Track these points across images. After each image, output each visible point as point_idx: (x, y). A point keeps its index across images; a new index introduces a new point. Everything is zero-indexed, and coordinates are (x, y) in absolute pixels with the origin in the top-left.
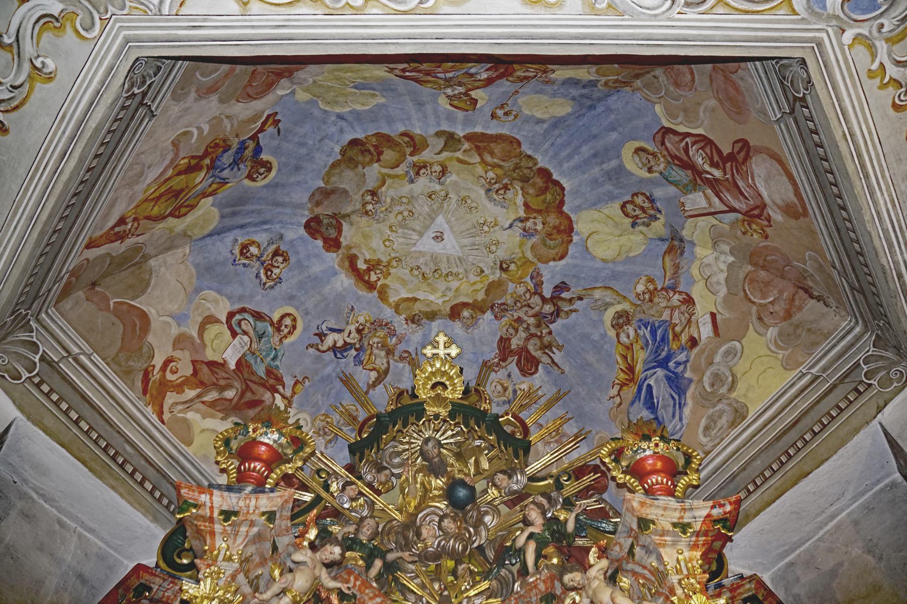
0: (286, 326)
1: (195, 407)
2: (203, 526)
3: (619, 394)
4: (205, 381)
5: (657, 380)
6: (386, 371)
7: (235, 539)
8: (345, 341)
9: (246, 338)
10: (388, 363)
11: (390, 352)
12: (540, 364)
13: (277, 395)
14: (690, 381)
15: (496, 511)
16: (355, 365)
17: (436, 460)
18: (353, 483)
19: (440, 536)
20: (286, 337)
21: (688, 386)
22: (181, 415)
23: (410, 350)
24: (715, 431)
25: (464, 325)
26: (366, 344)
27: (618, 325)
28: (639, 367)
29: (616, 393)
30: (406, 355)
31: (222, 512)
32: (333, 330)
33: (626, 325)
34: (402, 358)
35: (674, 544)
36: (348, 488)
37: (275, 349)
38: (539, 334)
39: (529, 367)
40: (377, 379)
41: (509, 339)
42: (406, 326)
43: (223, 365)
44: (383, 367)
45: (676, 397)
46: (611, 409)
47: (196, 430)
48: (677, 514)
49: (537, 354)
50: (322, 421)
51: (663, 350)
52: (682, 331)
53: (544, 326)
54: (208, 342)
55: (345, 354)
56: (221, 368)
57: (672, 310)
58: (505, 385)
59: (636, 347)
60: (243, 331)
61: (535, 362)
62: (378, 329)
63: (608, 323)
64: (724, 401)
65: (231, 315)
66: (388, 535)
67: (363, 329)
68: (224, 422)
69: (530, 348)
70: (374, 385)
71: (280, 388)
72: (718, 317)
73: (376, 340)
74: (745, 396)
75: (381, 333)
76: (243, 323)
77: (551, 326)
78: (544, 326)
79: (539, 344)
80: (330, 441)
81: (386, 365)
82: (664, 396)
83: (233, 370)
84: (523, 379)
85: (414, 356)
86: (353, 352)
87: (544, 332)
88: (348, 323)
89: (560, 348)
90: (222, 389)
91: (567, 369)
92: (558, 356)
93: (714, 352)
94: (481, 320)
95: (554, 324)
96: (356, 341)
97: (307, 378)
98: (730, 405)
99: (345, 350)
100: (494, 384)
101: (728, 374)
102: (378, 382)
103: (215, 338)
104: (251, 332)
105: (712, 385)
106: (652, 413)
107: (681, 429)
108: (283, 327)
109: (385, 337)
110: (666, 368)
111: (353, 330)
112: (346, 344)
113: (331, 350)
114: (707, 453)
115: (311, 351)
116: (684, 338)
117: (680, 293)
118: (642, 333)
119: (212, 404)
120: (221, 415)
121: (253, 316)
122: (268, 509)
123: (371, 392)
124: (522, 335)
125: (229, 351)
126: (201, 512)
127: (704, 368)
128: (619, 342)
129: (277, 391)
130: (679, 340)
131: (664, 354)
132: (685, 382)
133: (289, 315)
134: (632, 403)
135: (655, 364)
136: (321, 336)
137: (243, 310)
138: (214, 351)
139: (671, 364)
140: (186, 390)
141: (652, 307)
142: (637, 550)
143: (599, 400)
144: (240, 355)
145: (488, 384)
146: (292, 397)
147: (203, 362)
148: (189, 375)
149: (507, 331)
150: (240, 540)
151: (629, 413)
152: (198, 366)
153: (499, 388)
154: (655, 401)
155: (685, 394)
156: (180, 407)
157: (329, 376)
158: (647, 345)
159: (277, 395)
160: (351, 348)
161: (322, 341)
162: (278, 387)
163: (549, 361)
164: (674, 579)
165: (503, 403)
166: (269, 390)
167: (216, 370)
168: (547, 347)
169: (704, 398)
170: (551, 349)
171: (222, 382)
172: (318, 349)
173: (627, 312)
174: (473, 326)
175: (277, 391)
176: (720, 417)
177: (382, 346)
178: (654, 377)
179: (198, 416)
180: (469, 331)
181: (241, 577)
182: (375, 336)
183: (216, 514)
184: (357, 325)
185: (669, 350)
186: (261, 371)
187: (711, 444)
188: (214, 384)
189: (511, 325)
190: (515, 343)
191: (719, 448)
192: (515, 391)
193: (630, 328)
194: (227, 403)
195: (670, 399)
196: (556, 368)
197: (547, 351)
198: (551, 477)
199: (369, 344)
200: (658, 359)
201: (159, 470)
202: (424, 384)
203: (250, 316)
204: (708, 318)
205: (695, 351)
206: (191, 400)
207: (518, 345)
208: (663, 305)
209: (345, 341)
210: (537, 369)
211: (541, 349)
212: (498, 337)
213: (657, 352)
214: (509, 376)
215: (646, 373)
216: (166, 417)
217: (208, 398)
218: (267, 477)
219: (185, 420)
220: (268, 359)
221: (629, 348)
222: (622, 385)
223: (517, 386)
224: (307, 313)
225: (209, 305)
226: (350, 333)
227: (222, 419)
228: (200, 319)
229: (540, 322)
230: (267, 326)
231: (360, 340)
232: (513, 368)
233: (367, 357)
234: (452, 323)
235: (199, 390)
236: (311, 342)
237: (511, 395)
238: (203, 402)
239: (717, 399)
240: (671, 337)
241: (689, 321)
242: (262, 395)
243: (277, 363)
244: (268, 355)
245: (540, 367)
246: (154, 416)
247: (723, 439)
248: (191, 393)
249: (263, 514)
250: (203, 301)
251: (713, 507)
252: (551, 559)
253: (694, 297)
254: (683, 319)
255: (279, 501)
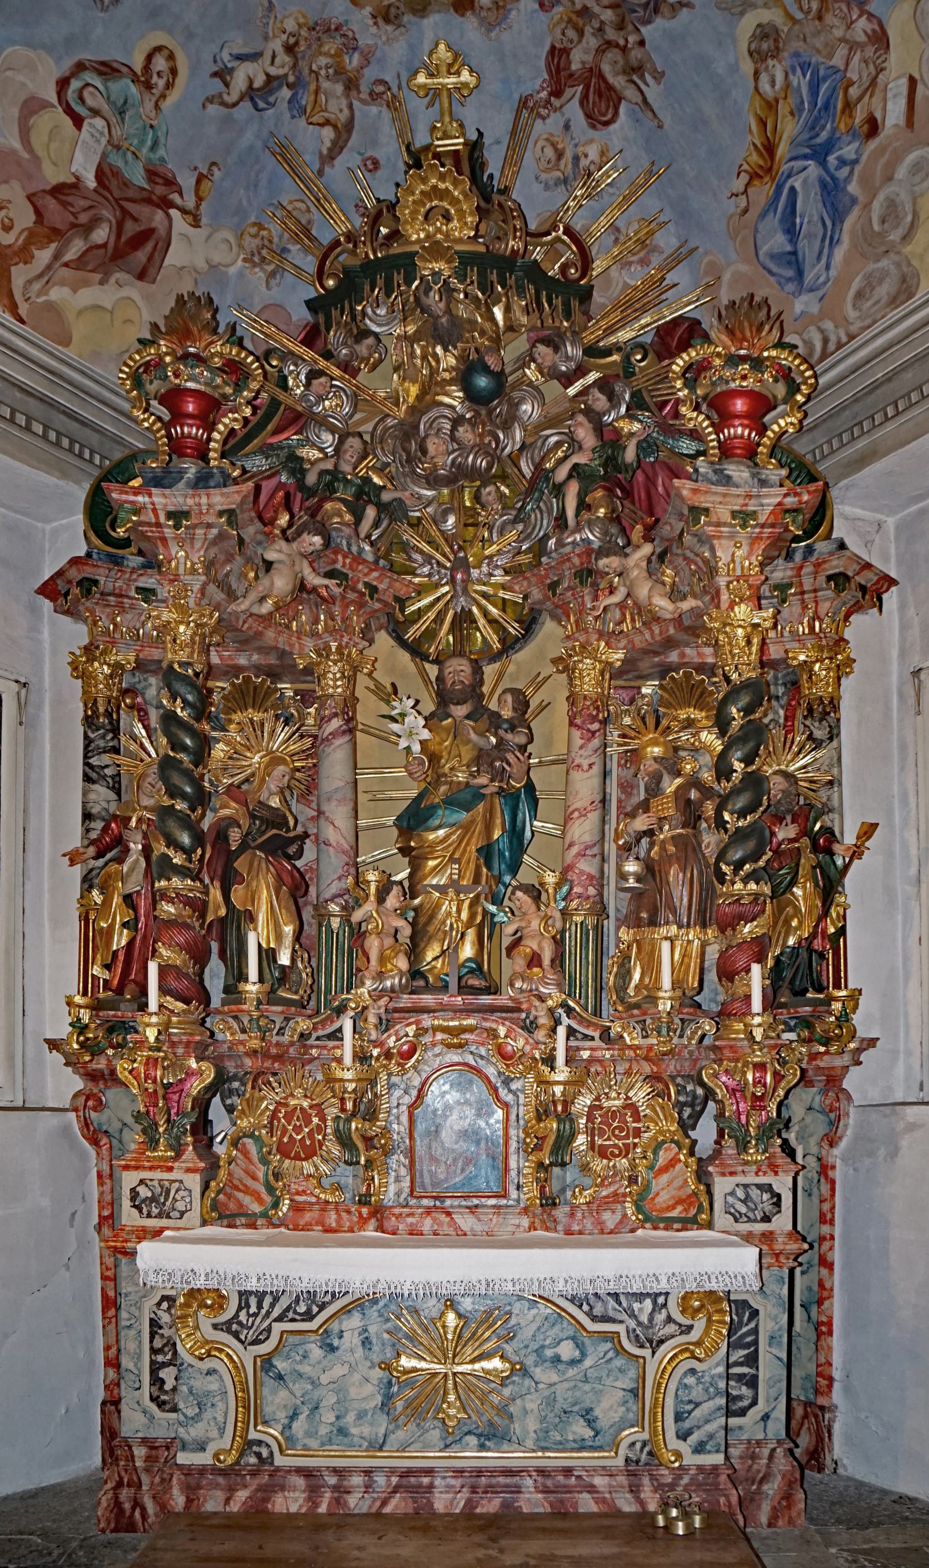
0: (159, 74)
1: (56, 277)
2: (151, 532)
3: (745, 191)
4: (58, 226)
5: (805, 181)
6: (349, 126)
7: (192, 543)
8: (267, 75)
9: (99, 123)
10: (350, 106)
11: (351, 85)
12: (623, 102)
13: (173, 212)
14: (854, 201)
15: (538, 393)
16: (293, 117)
17: (444, 320)
18: (321, 373)
19: (454, 451)
20: (163, 96)
21: (847, 211)
22: (42, 299)
23: (387, 79)
24: (869, 304)
25: (482, 20)
26: (306, 71)
27: (758, 53)
28: (782, 150)
29: (742, 189)
30: (381, 88)
31: (170, 515)
32: (240, 58)
33: (773, 57)
34: (374, 96)
35: (732, 536)
36: (315, 382)
37: (152, 126)
38: (622, 42)
39: (603, 109)
40: (334, 143)
41: (566, 52)
42: (374, 30)
43: (76, 185)
44: (344, 116)
45: (829, 224)
46: (732, 216)
47: (70, 316)
48: (741, 501)
49: (618, 81)
50: (255, 236)
51: (824, 127)
52: (860, 99)
53: (630, 27)
54: (41, 153)
55: (271, 99)
56: (74, 191)
57: (850, 49)
58: (560, 146)
59: (783, 109)
60: (91, 110)
61: (611, 97)
62: (324, 38)
63: (744, 46)
64: (892, 255)
65: (63, 84)
66: (381, 442)
67: (297, 43)
68: (105, 287)
69: (606, 68)
70: (330, 157)
71: (175, 197)
72: (920, 88)
73: (323, 61)
74: (921, 257)
75: (331, 46)
76: (86, 94)
77: (643, 30)
78: (630, 27)
79: (621, 62)
80: (272, 274)
81: (346, 111)
82: (811, 216)
83: (95, 190)
84: (592, 133)
85: (395, 89)
86: (285, 93)
87: (631, 39)
88: (266, 38)
89: (659, 76)
90: (87, 229)
91: (667, 120)
92: (653, 92)
93: (898, 158)
94: (514, 13)
95: (649, 27)
96: (286, 70)
97: (214, 164)
98: (898, 265)
99: (271, 92)
100: (541, 143)
101: (908, 207)
102: (337, 149)
103: (50, 140)
104: (105, 108)
105: (883, 221)
106: (791, 241)
107: (825, 283)
108: (155, 79)
109: (338, 54)
110: (823, 163)
111: (280, 50)
112: (270, 78)
113: (247, 99)
114: (851, 337)
115: (212, 109)
116: (860, 115)
117: (871, 16)
118: (795, 83)
119: (80, 264)
120: (97, 277)
121: (100, 73)
122: (225, 507)
123: (327, 170)
124: (591, 41)
125: (79, 156)
126: (143, 518)
127: (878, 184)
128: (756, 89)
129: (172, 205)
130: (851, 116)
131: (824, 135)
132: (846, 199)
133: (158, 49)
134: (763, 215)
135: (807, 151)
136: (223, 75)
137: (80, 67)
138: (55, 164)
139: (832, 159)
140: (36, 252)
141: (819, 32)
142: (687, 538)
143: (715, 194)
144: (96, 159)
145: (530, 145)
146: (198, 206)
147: (44, 191)
148: (31, 225)
149: (563, 34)
150: (198, 545)
151: (756, 230)
152: (39, 203)
153: (549, 152)
154: (798, 221)
155: (842, 222)
156: (37, 286)
157: (251, 148)
158: (801, 110)
159: (173, 212)
160: (280, 87)
161: (227, 85)
162: (171, 196)
163: (639, 99)
164: (722, 581)
165: (556, 184)
166: (158, 206)
167: (70, 199)
168: (634, 70)
169: (865, 240)
170: (642, 77)
171: (83, 218)
172: (224, 104)
173: (777, 31)
174: (499, 24)
175: (172, 205)
176: (881, 281)
177: (336, 72)
178: (803, 175)
179: (66, 291)
180: (493, 35)
181: (212, 588)
182: (321, 54)
183: (162, 519)
184: (284, 37)
185: (834, 130)
186: (138, 177)
187: (859, 324)
188: (74, 226)
189: (570, 21)
190: (578, 59)
191: (868, 334)
192: (576, 159)
193: (778, 66)
194: (102, 251)
195: (820, 225)
196: (650, 114)
197: (635, 78)
198: (619, 349)
199: (311, 71)
200: (813, 142)
201: (42, 399)
202: (414, 213)
203: (94, 75)
204: (904, 82)
205: (873, 144)
206: (49, 267)
207: (583, 63)
208: (838, 33)
209: (267, 75)
210: (616, 113)
211: (624, 72)
212: (547, 48)
213: (813, 127)
214: (567, 127)
215: (792, 163)
216: (23, 310)
217: (71, 255)
218: (209, 439)
219: (50, 307)
220: (145, 151)
221: (771, 106)
222: (754, 176)
223: (580, 149)
224: (190, 36)
225: (20, 78)
226: (274, 57)
227: (101, 283)
228: (15, 112)
229: (623, 20)
230: (128, 86)
231: (294, 66)
232: (574, 110)
233: (312, 98)
234: (460, 19)
235: (54, 246)
236: (211, 92)
237: (570, 166)
238: (66, 265)
239: (884, 249)
240: (840, 106)
241: (873, 82)
242: (151, 219)
243: (161, 152)
244: (142, 142)
245: (622, 110)
246: (7, 316)
247: (875, 322)
248: (43, 256)
249: (221, 514)
250: (9, 73)
251: (785, 495)
252: (597, 510)
253: (891, 33)
254: (865, 75)
255: (238, 498)
